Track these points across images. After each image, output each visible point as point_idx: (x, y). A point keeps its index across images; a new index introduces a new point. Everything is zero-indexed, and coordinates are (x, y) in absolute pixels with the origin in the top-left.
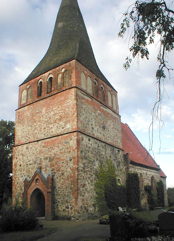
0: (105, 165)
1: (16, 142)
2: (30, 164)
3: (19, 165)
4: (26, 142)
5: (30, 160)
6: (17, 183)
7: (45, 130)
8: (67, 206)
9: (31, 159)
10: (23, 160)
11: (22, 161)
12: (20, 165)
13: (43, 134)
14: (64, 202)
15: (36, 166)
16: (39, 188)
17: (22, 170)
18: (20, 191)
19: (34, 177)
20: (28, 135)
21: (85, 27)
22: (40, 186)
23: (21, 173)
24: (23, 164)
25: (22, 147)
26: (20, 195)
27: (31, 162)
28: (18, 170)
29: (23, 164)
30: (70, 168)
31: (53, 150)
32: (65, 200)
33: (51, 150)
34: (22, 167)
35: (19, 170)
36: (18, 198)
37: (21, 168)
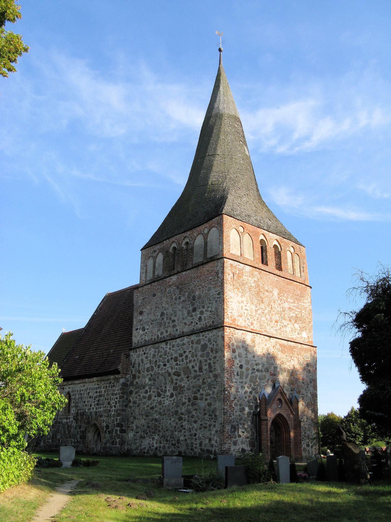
0: (184, 371)
1: (227, 319)
2: (258, 370)
3: (239, 365)
4: (245, 327)
5: (259, 364)
6: (235, 398)
7: (277, 325)
8: (307, 443)
9: (260, 363)
10: (246, 358)
11: (244, 359)
12: (241, 367)
13: (275, 329)
14: (305, 438)
15: (267, 375)
16: (282, 413)
17: (244, 377)
18: (240, 413)
19: (285, 396)
20: (251, 318)
21: (202, 128)
22: (283, 410)
23: (241, 380)
24: (247, 366)
25: (242, 334)
26: (240, 420)
27: (260, 367)
28: (236, 374)
29: (247, 366)
30: (311, 393)
31: (292, 361)
32: (307, 435)
33: (290, 359)
34: (244, 369)
35: (238, 375)
36: (238, 425)
37: (242, 373)
